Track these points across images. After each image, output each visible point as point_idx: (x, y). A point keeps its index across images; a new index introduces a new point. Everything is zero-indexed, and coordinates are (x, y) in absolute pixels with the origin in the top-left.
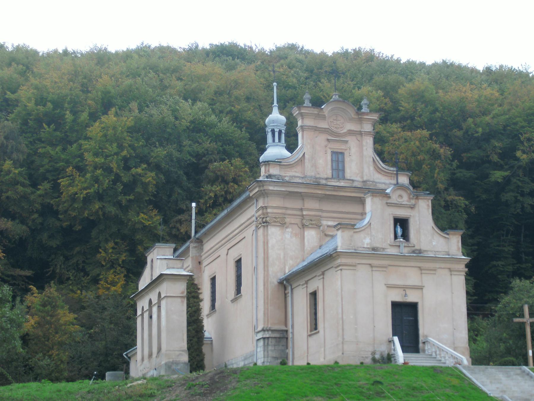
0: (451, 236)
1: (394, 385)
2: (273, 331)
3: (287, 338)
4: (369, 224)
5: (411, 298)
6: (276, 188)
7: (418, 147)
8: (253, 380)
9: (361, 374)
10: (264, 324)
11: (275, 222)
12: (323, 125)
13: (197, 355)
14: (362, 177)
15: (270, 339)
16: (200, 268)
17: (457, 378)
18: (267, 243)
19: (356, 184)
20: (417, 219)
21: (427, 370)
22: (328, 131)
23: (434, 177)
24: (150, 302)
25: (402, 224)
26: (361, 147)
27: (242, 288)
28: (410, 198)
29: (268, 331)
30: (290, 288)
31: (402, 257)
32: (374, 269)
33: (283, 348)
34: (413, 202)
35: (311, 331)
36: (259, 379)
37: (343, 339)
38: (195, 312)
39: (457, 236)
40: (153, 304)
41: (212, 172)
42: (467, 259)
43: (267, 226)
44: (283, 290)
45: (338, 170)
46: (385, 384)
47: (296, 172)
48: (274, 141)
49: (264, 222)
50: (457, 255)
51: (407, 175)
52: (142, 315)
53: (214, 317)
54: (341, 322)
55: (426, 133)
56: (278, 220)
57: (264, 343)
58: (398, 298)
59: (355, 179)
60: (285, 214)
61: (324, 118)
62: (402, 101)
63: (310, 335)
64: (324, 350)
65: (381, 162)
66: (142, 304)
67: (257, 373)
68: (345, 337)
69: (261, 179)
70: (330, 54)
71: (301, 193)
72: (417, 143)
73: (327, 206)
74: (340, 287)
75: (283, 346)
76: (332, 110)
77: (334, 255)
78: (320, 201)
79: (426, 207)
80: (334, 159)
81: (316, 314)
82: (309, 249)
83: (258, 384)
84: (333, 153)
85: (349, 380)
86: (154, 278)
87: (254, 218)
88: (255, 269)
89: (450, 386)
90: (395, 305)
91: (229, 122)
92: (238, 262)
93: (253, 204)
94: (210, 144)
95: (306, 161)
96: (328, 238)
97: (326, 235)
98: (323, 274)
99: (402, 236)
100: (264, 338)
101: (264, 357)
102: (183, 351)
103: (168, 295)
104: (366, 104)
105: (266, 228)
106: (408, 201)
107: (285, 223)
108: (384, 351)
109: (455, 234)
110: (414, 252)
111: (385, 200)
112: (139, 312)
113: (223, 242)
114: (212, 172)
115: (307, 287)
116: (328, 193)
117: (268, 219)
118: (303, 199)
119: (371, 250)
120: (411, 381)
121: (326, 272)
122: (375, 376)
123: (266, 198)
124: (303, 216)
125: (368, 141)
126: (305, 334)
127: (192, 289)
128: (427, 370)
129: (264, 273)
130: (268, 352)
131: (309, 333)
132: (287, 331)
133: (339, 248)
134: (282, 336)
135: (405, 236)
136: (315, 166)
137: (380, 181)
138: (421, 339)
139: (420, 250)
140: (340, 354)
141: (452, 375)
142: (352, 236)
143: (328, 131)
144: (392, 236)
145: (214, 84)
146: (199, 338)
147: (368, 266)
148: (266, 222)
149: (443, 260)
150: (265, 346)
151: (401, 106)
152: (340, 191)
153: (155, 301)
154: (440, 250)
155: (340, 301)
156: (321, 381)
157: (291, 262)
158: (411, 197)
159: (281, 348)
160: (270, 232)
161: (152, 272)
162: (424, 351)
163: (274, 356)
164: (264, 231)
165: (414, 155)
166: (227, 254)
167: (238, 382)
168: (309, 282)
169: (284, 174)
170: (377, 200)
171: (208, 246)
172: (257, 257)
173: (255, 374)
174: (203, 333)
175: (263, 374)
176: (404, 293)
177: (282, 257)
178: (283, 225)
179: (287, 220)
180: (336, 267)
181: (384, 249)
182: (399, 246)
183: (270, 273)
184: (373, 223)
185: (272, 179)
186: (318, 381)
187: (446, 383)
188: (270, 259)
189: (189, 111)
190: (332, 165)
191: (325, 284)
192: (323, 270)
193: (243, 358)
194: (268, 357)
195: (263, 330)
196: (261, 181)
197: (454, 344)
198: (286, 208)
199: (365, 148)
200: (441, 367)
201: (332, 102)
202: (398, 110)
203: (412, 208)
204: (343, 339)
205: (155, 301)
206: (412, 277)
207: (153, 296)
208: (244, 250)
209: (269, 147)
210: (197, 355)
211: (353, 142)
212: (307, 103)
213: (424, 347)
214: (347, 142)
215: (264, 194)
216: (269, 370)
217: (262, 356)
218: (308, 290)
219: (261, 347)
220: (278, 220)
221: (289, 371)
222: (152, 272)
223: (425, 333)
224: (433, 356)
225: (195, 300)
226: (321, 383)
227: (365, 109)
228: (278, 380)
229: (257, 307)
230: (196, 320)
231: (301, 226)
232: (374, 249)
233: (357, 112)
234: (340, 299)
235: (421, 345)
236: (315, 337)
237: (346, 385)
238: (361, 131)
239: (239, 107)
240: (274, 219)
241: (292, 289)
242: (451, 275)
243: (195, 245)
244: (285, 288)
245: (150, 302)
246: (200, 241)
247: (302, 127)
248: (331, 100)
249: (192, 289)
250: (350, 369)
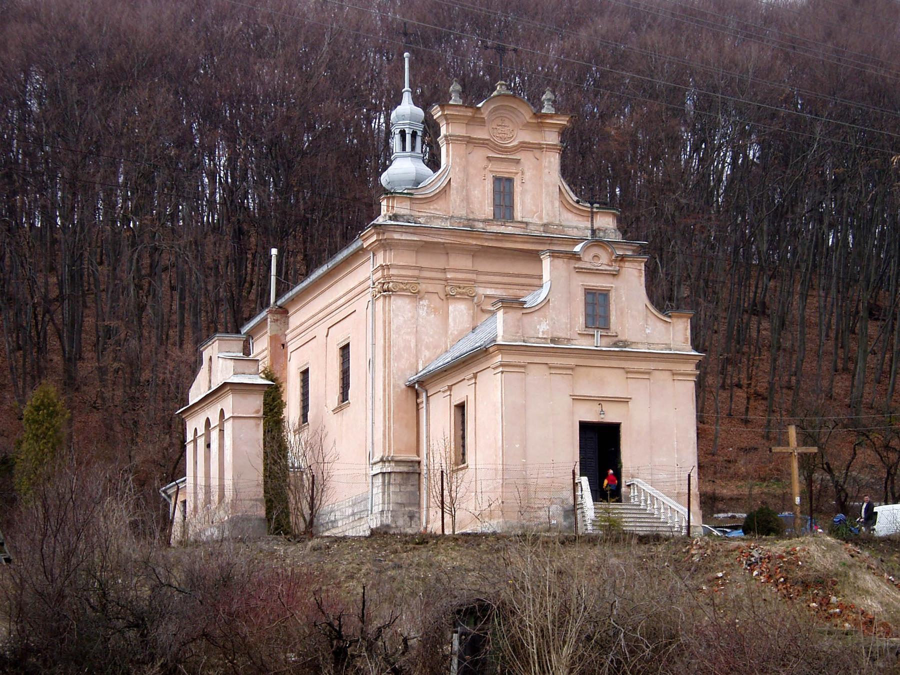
0: (675, 320)
2: (398, 462)
3: (419, 474)
4: (547, 301)
5: (611, 416)
10: (384, 451)
11: (404, 290)
12: (480, 134)
14: (541, 218)
24: (208, 422)
30: (424, 394)
40: (212, 426)
43: (390, 296)
47: (436, 209)
48: (404, 149)
51: (613, 214)
52: (195, 441)
56: (408, 287)
58: (591, 415)
59: (530, 220)
61: (482, 122)
65: (571, 193)
66: (194, 425)
71: (444, 243)
73: (486, 265)
77: (491, 350)
79: (636, 273)
81: (463, 438)
86: (214, 388)
87: (370, 282)
88: (371, 363)
90: (585, 427)
92: (345, 350)
93: (369, 258)
96: (487, 316)
97: (483, 311)
98: (475, 376)
100: (384, 473)
101: (383, 503)
102: (256, 500)
103: (235, 415)
104: (549, 100)
109: (681, 317)
112: (190, 437)
113: (321, 315)
116: (486, 244)
125: (552, 159)
129: (385, 372)
130: (389, 495)
132: (419, 462)
136: (467, 199)
137: (571, 224)
152: (508, 241)
153: (215, 422)
157: (427, 353)
159: (410, 488)
160: (393, 306)
161: (210, 376)
162: (628, 499)
164: (384, 304)
171: (296, 319)
172: (374, 344)
177: (413, 345)
178: (416, 296)
181: (569, 340)
185: (397, 221)
195: (382, 461)
196: (380, 225)
198: (421, 269)
201: (494, 97)
203: (614, 275)
205: (215, 422)
206: (612, 383)
207: (212, 412)
214: (518, 161)
220: (408, 287)
222: (210, 376)
227: (547, 109)
231: (443, 297)
235: (623, 489)
240: (402, 286)
241: (428, 397)
244: (418, 396)
245: (208, 422)
246: (283, 312)
247: (446, 136)
248: (495, 93)
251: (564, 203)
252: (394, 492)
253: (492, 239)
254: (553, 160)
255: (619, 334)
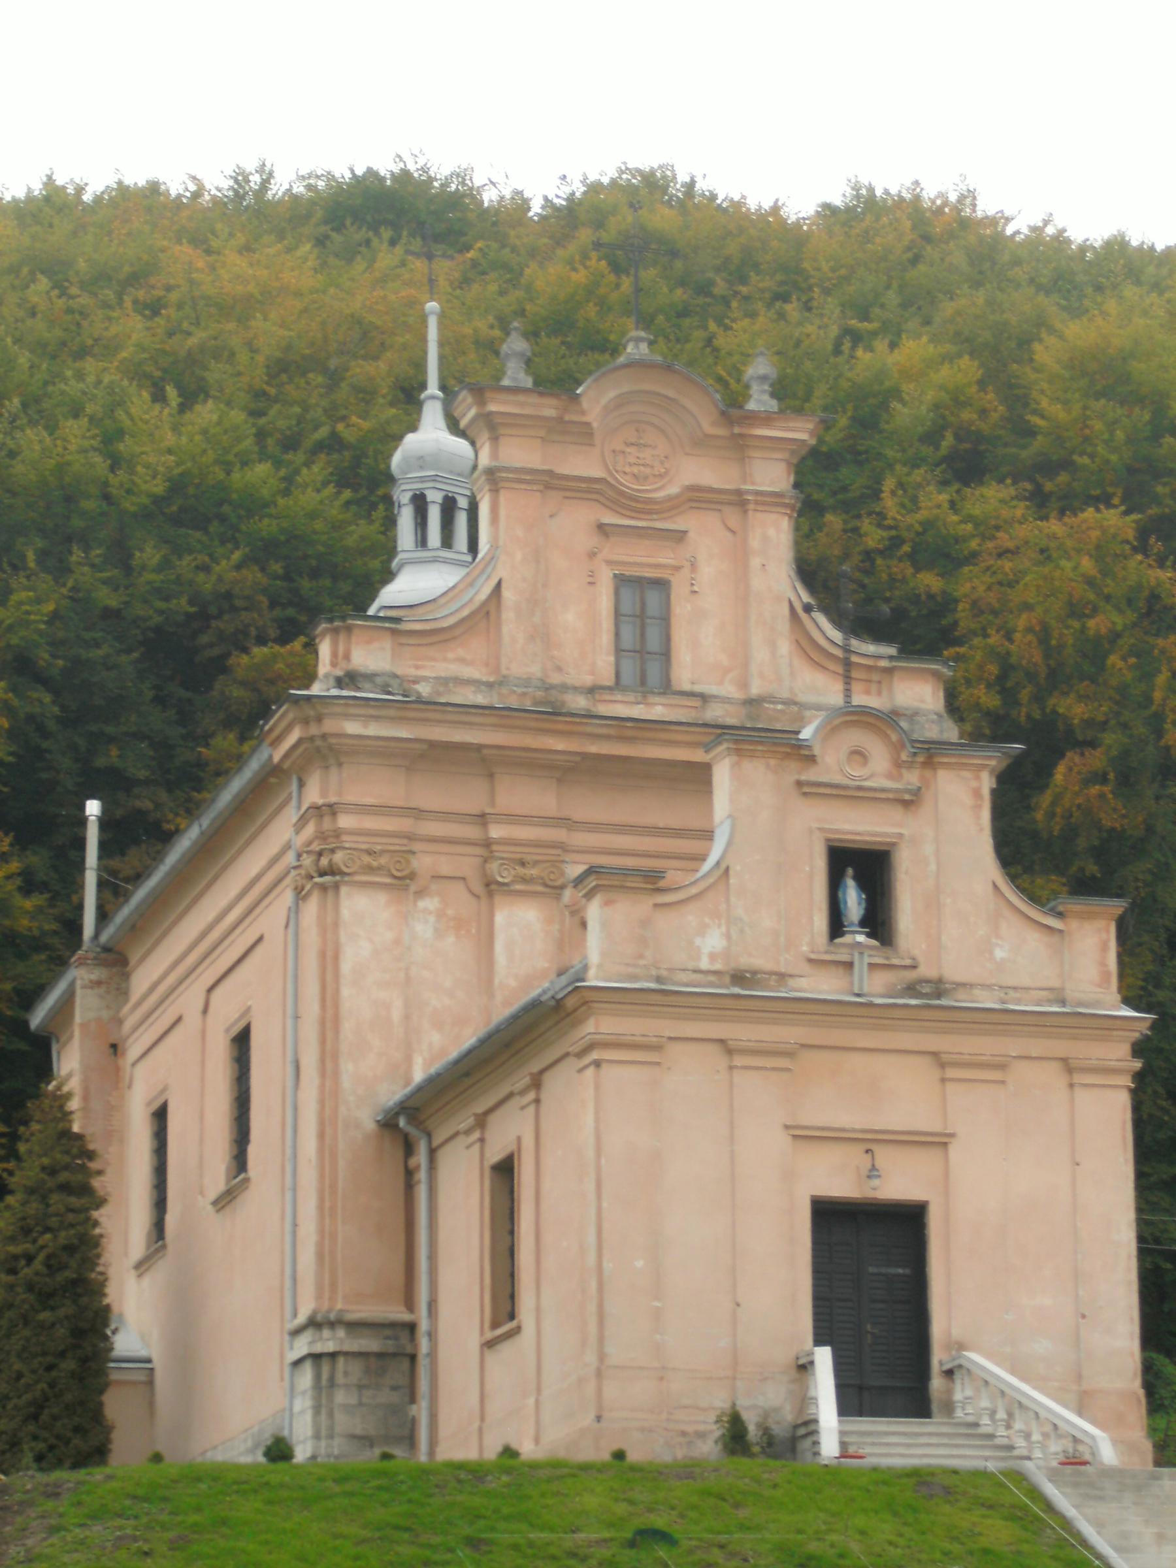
0: (1074, 924)
1: (722, 1547)
2: (354, 1326)
3: (413, 1358)
5: (898, 1183)
6: (373, 730)
7: (1090, 582)
8: (119, 1522)
9: (591, 1502)
10: (319, 1296)
11: (370, 869)
12: (581, 464)
13: (77, 1429)
14: (744, 684)
15: (341, 1361)
16: (118, 1070)
17: (1011, 1518)
18: (336, 958)
19: (715, 713)
20: (928, 849)
21: (885, 1483)
22: (598, 492)
23: (1149, 700)
25: (864, 871)
26: (740, 557)
27: (252, 1150)
28: (898, 764)
29: (332, 1325)
31: (858, 1011)
32: (739, 1061)
33: (395, 1398)
34: (912, 778)
35: (495, 1325)
36: (144, 1520)
37: (602, 1356)
38: (70, 1249)
39: (1100, 923)
41: (243, 684)
42: (1139, 1020)
43: (336, 887)
44: (400, 1153)
45: (641, 652)
46: (685, 1544)
47: (462, 661)
48: (422, 542)
49: (324, 875)
50: (1097, 1004)
51: (936, 674)
53: (161, 1270)
54: (593, 1285)
55: (1115, 521)
56: (383, 860)
57: (317, 1377)
58: (842, 1186)
60: (411, 837)
61: (584, 434)
62: (1042, 392)
63: (490, 1344)
64: (537, 1402)
67: (141, 1492)
68: (610, 1349)
69: (316, 689)
70: (753, 207)
71: (479, 748)
72: (1087, 565)
73: (590, 805)
74: (591, 1141)
75: (394, 1388)
76: (621, 402)
77: (570, 1003)
78: (559, 781)
79: (968, 800)
80: (626, 608)
82: (513, 983)
83: (135, 1539)
84: (621, 581)
85: (532, 1525)
89: (971, 1553)
90: (828, 1215)
91: (325, 484)
93: (289, 798)
94: (238, 567)
95: (508, 615)
98: (536, 1083)
99: (863, 923)
100: (316, 1357)
101: (317, 1436)
104: (763, 378)
105: (331, 894)
106: (889, 776)
107: (412, 876)
108: (777, 1410)
110: (911, 989)
111: (793, 772)
114: (243, 684)
115: (482, 1140)
116: (593, 749)
117: (338, 857)
118: (491, 776)
119: (727, 979)
120: (799, 1532)
121: (547, 1077)
122: (650, 1510)
123: (334, 773)
124: (488, 844)
125: (771, 532)
126: (473, 1341)
127: (58, 1156)
128: (885, 1483)
129: (322, 1087)
130: (331, 1415)
131: (489, 1335)
132: (412, 1327)
133: (592, 973)
134: (390, 1346)
135: (878, 923)
136: (543, 635)
138: (939, 1357)
139: (940, 981)
140: (588, 1419)
141: (991, 1507)
142: (645, 923)
143: (598, 492)
144: (821, 921)
145: (270, 332)
146: (84, 1361)
147: (714, 1049)
148: (331, 871)
149: (1037, 1023)
150: (323, 1390)
151: (1035, 412)
154: (1026, 981)
155: (592, 1196)
156: (407, 1529)
157: (436, 1038)
158: (904, 756)
159: (386, 1397)
160: (345, 913)
162: (949, 1407)
163: (358, 1431)
164: (323, 907)
165: (1076, 610)
166: (205, 1011)
167: (53, 1530)
168: (493, 1119)
169: (412, 672)
170: (758, 771)
171: (142, 979)
173: (135, 1497)
174: (106, 1338)
175: (165, 1499)
176: (865, 1162)
177: (396, 1015)
178: (402, 882)
179: (423, 862)
180: (580, 1054)
181: (782, 977)
182: (849, 965)
183: (346, 1083)
184: (736, 868)
185: (358, 689)
186: (397, 1528)
187: (954, 1539)
188: (347, 1027)
189: (166, 441)
190: (617, 635)
191: (544, 1125)
192: (535, 1067)
193: (250, 1444)
194: (331, 1436)
195: (314, 1323)
197: (1079, 1377)
198: (419, 813)
199: (755, 562)
200: (955, 1472)
202: (1030, 432)
203: (907, 804)
204: (602, 1356)
206: (904, 1095)
208: (255, 993)
209: (401, 566)
210: (77, 1429)
211: (706, 536)
212: (515, 374)
213: (950, 1392)
214: (680, 536)
215: (324, 753)
216: (199, 1479)
217: (309, 1433)
218: (488, 1154)
219: (304, 1393)
220: (383, 860)
221: (282, 1485)
223: (956, 1333)
224: (983, 1430)
225: (73, 1201)
226: (406, 1536)
227: (759, 400)
228: (224, 1522)
229: (295, 1225)
230: (74, 1283)
231: (478, 887)
232: (738, 978)
233: (723, 413)
234: (591, 1187)
235: (937, 1383)
236: (506, 1350)
237: (516, 1547)
238: (739, 492)
239: (366, 425)
240: (367, 859)
241: (432, 1152)
242: (1071, 1086)
243: (97, 974)
244: (409, 1149)
246: (116, 960)
248: (622, 360)
249: (58, 1156)
250: (549, 1481)
251: (809, 649)
252: (347, 1408)
253: (608, 737)
254: (774, 538)
255: (921, 959)
